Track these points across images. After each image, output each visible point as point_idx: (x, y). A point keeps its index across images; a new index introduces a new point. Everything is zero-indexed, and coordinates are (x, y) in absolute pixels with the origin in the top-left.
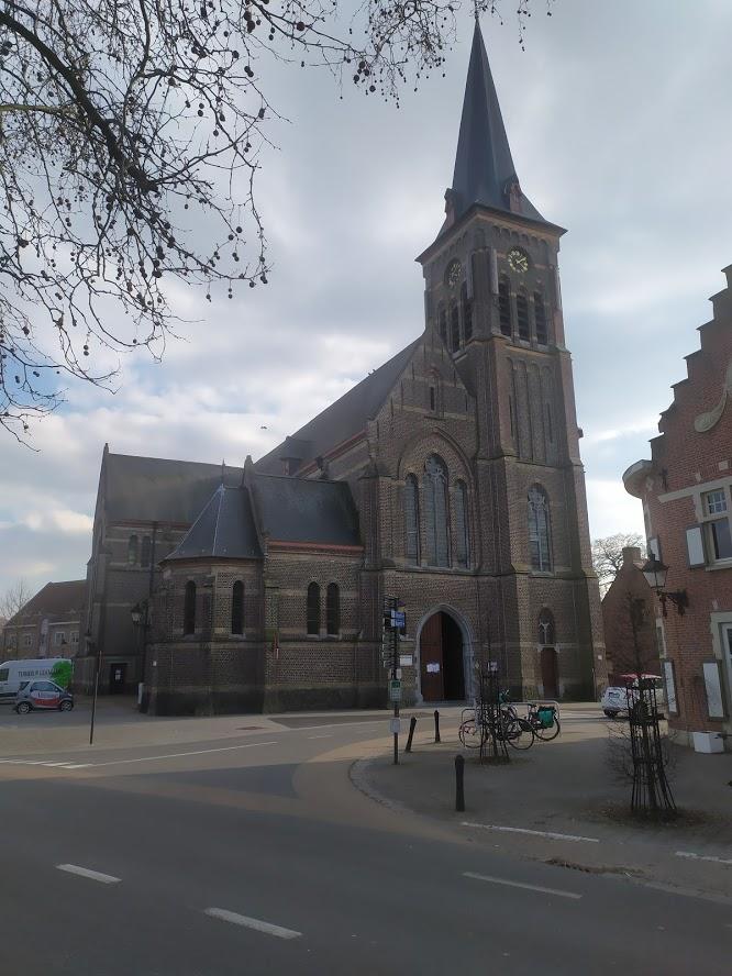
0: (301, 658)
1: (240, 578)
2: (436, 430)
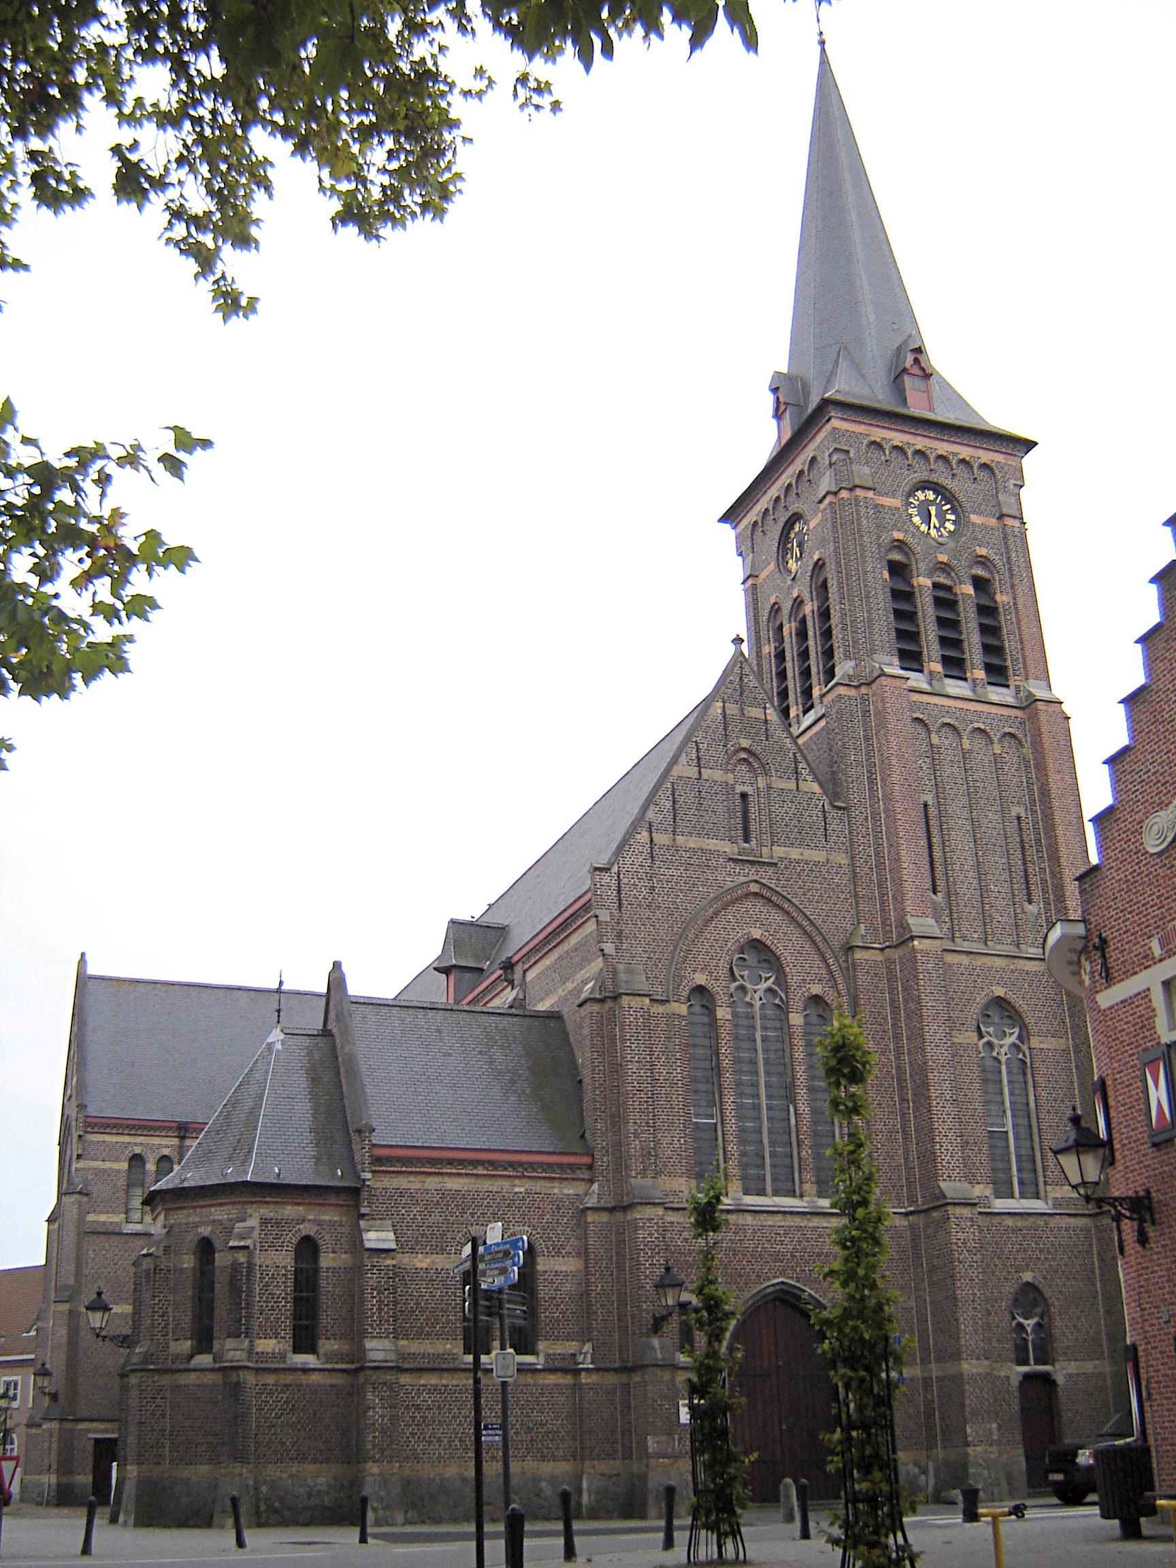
1: (307, 1229)
2: (754, 888)
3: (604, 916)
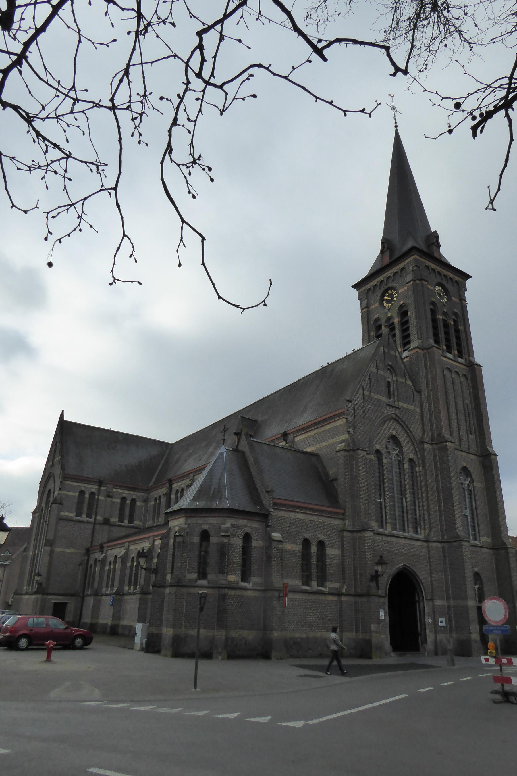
0: (304, 611)
1: (248, 530)
2: (394, 416)
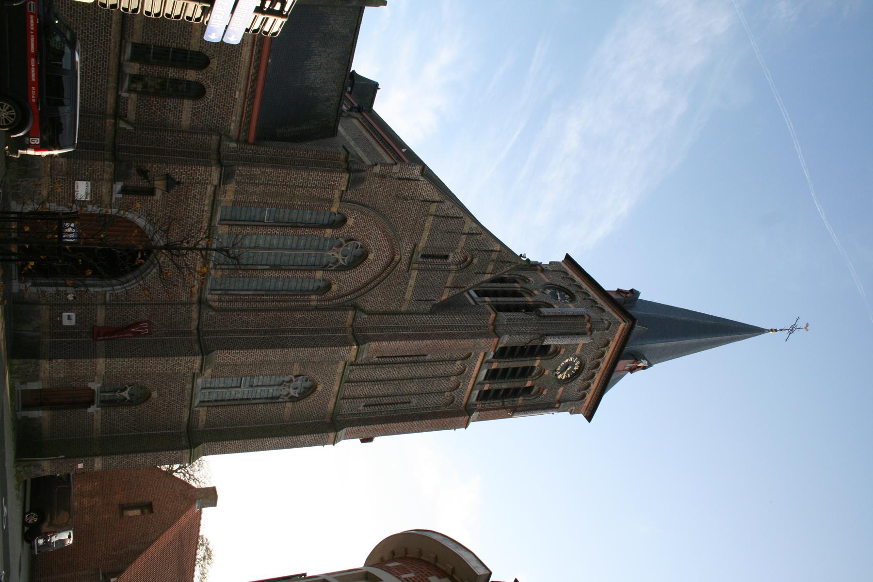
2: (397, 258)
3: (395, 169)
